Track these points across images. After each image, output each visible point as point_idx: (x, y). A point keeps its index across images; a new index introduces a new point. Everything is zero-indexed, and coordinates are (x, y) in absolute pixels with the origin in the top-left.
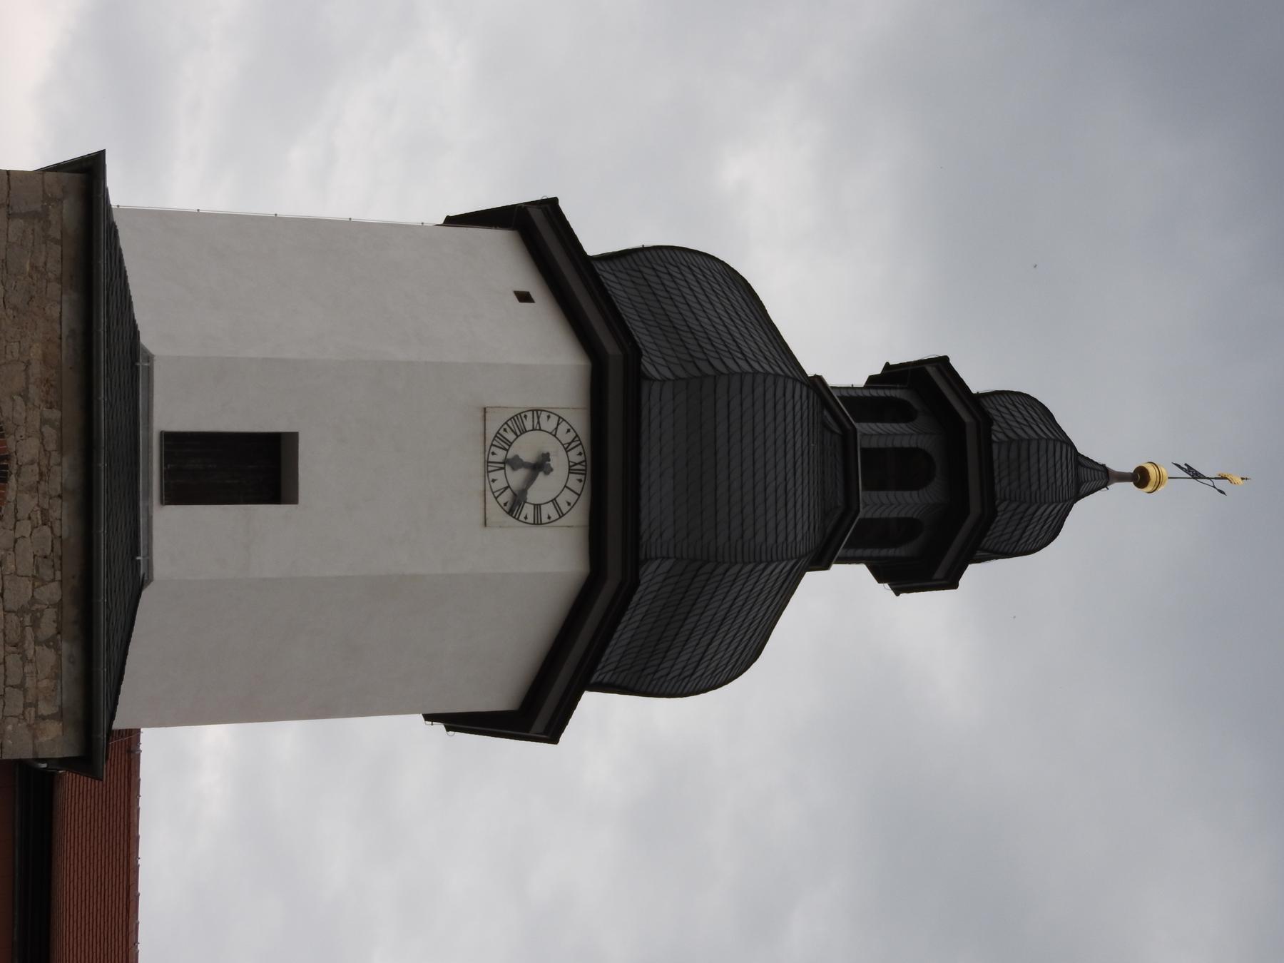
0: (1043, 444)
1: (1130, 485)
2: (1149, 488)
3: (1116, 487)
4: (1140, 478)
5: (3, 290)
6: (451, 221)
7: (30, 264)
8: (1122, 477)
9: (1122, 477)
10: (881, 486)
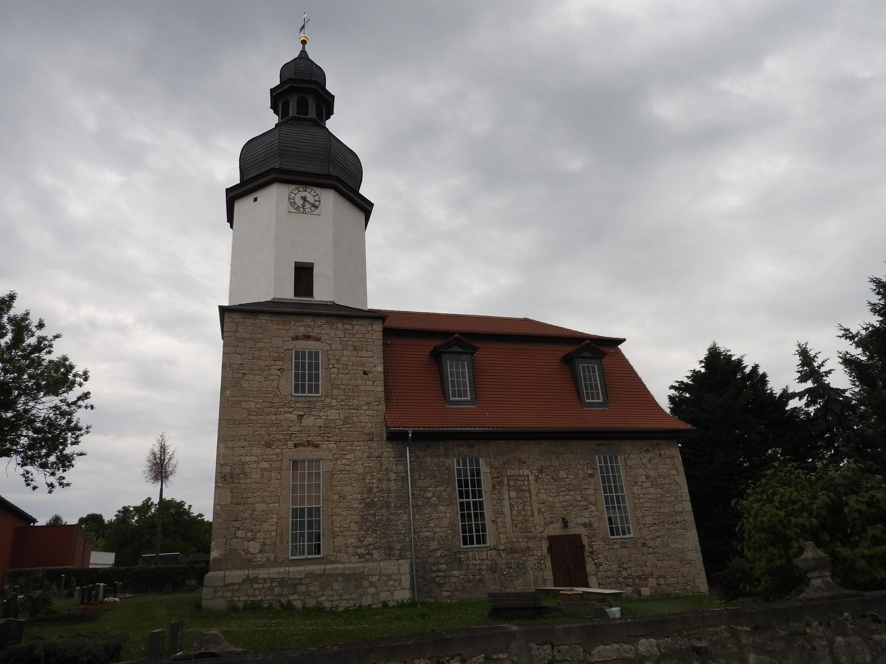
4: (304, 42)
6: (232, 227)
8: (304, 47)
9: (304, 47)
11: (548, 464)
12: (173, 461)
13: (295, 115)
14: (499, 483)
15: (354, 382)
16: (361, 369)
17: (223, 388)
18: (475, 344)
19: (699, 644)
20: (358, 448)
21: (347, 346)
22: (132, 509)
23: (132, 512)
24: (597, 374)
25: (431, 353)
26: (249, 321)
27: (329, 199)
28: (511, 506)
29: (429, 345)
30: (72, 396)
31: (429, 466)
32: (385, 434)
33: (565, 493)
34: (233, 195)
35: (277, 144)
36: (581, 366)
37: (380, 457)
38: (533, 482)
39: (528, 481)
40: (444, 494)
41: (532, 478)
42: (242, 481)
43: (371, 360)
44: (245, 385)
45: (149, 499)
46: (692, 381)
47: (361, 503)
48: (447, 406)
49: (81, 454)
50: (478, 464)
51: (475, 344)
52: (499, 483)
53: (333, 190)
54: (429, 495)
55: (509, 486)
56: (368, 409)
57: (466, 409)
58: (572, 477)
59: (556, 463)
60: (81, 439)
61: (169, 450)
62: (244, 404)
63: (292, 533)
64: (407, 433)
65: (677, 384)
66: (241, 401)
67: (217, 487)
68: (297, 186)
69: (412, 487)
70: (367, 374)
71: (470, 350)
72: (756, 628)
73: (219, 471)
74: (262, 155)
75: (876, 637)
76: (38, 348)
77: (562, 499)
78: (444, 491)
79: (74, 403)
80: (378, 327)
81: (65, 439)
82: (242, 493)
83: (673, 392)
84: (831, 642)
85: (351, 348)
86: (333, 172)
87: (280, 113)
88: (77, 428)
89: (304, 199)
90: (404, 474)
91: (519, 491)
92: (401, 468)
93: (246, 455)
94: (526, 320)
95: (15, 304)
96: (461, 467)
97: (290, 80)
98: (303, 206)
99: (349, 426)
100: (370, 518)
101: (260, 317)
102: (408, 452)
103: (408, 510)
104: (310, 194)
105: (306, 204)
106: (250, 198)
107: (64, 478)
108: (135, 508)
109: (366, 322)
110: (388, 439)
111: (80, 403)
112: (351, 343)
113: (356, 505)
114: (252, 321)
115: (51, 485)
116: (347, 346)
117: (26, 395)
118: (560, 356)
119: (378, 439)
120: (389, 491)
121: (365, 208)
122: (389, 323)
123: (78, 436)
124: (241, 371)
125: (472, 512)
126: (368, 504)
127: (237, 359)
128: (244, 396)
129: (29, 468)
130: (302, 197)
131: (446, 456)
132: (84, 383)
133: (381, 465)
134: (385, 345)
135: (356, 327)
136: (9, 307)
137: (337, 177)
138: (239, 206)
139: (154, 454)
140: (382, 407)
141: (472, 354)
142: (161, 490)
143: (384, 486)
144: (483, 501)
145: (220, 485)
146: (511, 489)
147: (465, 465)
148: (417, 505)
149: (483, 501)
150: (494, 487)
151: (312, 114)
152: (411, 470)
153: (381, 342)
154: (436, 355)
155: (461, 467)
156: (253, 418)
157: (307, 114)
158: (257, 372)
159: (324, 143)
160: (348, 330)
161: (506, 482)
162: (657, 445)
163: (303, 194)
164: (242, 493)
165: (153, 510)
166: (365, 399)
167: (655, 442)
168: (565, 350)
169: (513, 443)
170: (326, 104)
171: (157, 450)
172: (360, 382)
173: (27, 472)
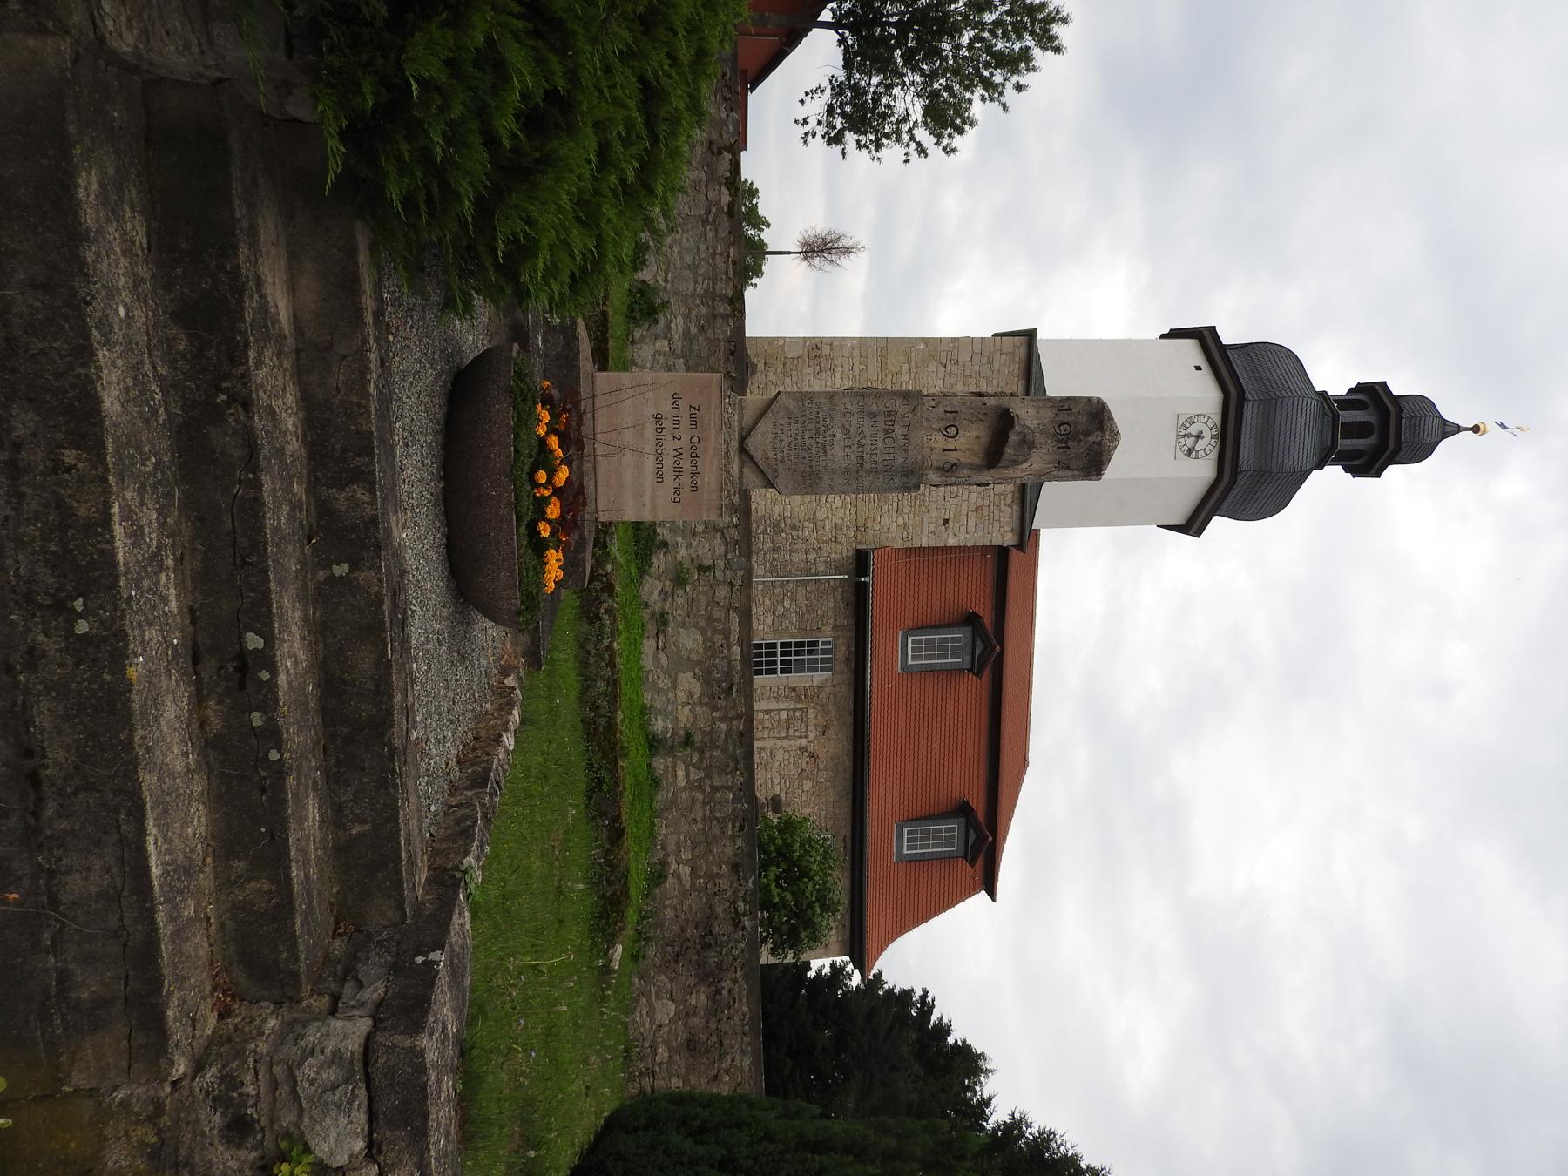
4: (1476, 429)
6: (1163, 336)
8: (1467, 429)
9: (1467, 429)
11: (822, 766)
12: (828, 267)
13: (1341, 419)
14: (798, 696)
15: (934, 506)
16: (952, 516)
17: (926, 341)
18: (986, 675)
19: (734, 690)
20: (848, 512)
21: (983, 498)
22: (754, 202)
23: (751, 203)
24: (943, 849)
25: (974, 613)
26: (1016, 369)
27: (1202, 471)
28: (769, 712)
29: (983, 607)
30: (922, 135)
31: (822, 604)
32: (864, 547)
33: (783, 786)
34: (1205, 338)
35: (1274, 396)
36: (955, 826)
37: (836, 541)
38: (798, 743)
39: (800, 737)
40: (787, 622)
41: (804, 742)
42: (811, 369)
43: (963, 529)
44: (931, 368)
45: (768, 226)
46: (935, 1025)
47: (780, 516)
48: (900, 633)
49: (844, 154)
50: (823, 669)
51: (986, 675)
52: (798, 696)
54: (787, 603)
55: (794, 710)
56: (897, 526)
57: (897, 657)
58: (804, 798)
59: (822, 777)
60: (864, 151)
61: (844, 260)
62: (906, 367)
64: (865, 575)
65: (929, 999)
66: (909, 362)
67: (805, 339)
68: (1219, 427)
69: (798, 581)
70: (944, 524)
71: (976, 669)
72: (742, 734)
73: (824, 341)
74: (1269, 375)
75: (730, 825)
76: (988, 85)
77: (776, 781)
78: (791, 623)
79: (912, 138)
80: (1009, 539)
81: (865, 133)
82: (797, 370)
83: (919, 993)
84: (729, 788)
85: (980, 503)
86: (1241, 479)
87: (1350, 397)
88: (878, 146)
89: (1199, 436)
90: (813, 571)
91: (788, 723)
92: (822, 568)
93: (843, 373)
94: (1024, 763)
95: (1049, 53)
96: (820, 647)
97: (1400, 411)
98: (1189, 435)
99: (876, 501)
100: (761, 528)
101: (1022, 382)
103: (769, 575)
104: (1208, 445)
105: (1193, 439)
106: (1201, 362)
107: (813, 137)
108: (756, 206)
109: (1016, 523)
110: (859, 551)
111: (913, 145)
112: (987, 503)
113: (778, 509)
114: (1016, 372)
115: (805, 122)
116: (983, 498)
117: (924, 83)
118: (970, 799)
119: (859, 537)
120: (792, 551)
121: (1193, 525)
122: (1015, 555)
123: (867, 147)
124: (948, 362)
125: (764, 659)
126: (778, 525)
127: (965, 356)
128: (917, 367)
129: (828, 92)
130: (1202, 432)
131: (835, 627)
132: (941, 148)
133: (825, 542)
134: (985, 549)
135: (1008, 510)
136: (1044, 48)
138: (1190, 347)
139: (838, 239)
140: (900, 544)
141: (970, 670)
142: (789, 253)
143: (800, 545)
144: (776, 673)
145: (808, 343)
146: (791, 713)
147: (824, 652)
148: (774, 587)
149: (776, 673)
150: (794, 690)
151: (1343, 444)
152: (819, 580)
153: (988, 543)
154: (971, 619)
155: (820, 647)
156: (889, 377)
157: (1344, 437)
158: (947, 382)
159: (1291, 462)
160: (1004, 499)
161: (800, 706)
162: (844, 926)
163: (1207, 434)
164: (797, 370)
165: (752, 232)
166: (911, 522)
167: (847, 923)
168: (979, 806)
169: (850, 720)
170: (1367, 465)
171: (844, 243)
172: (933, 514)
173: (822, 91)
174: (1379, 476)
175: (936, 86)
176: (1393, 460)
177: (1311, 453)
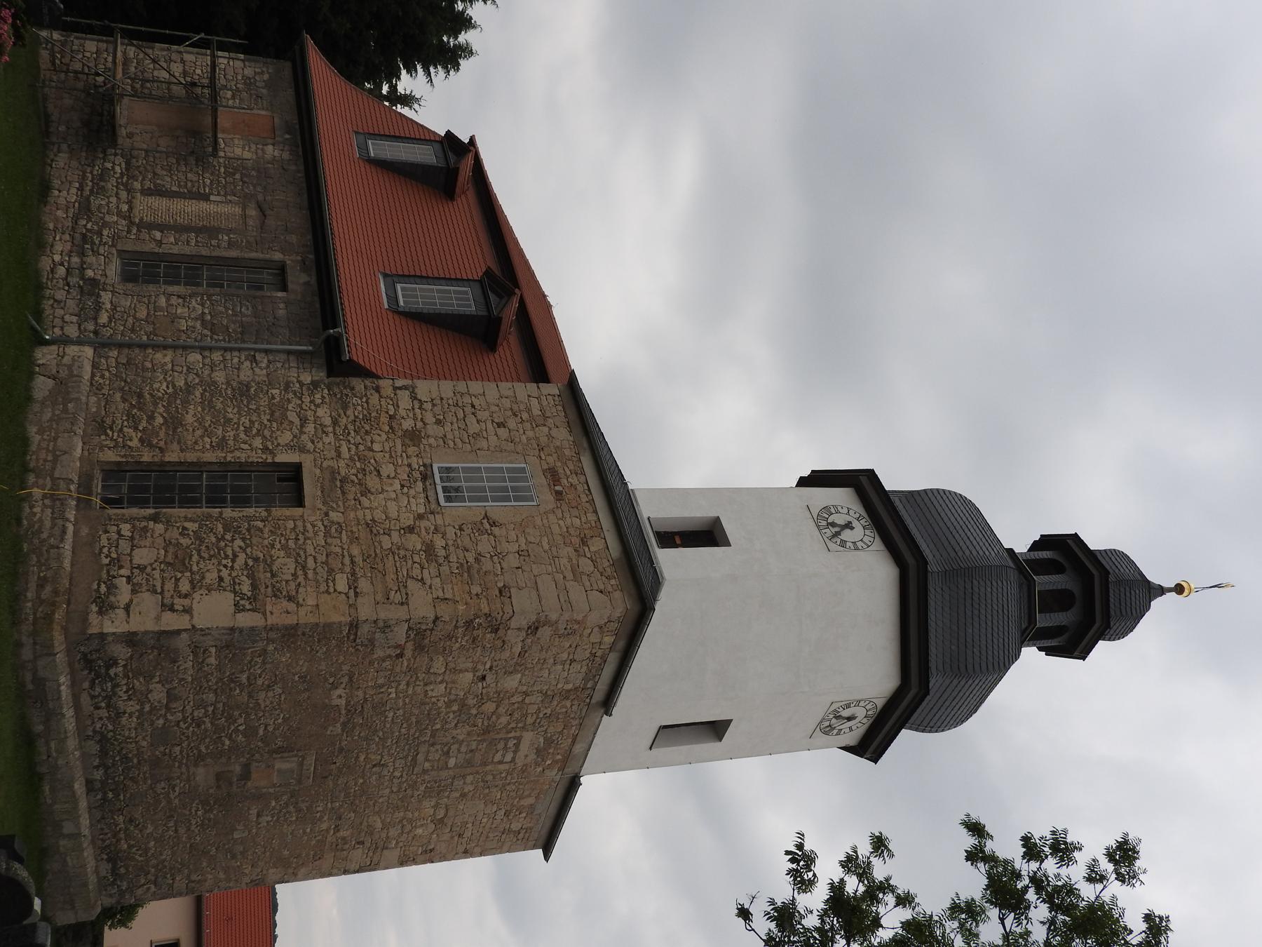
0: (967, 570)
1: (1174, 594)
2: (1185, 594)
3: (1168, 594)
4: (1179, 589)
5: (419, 397)
6: (803, 482)
7: (82, 780)
8: (1170, 590)
9: (1170, 590)
10: (1051, 610)
53: (899, 683)
63: (207, 507)
97: (1105, 573)
102: (238, 41)
137: (927, 693)
151: (1043, 621)
174: (1084, 658)
175: (125, 883)
176: (1101, 636)
177: (1015, 633)
